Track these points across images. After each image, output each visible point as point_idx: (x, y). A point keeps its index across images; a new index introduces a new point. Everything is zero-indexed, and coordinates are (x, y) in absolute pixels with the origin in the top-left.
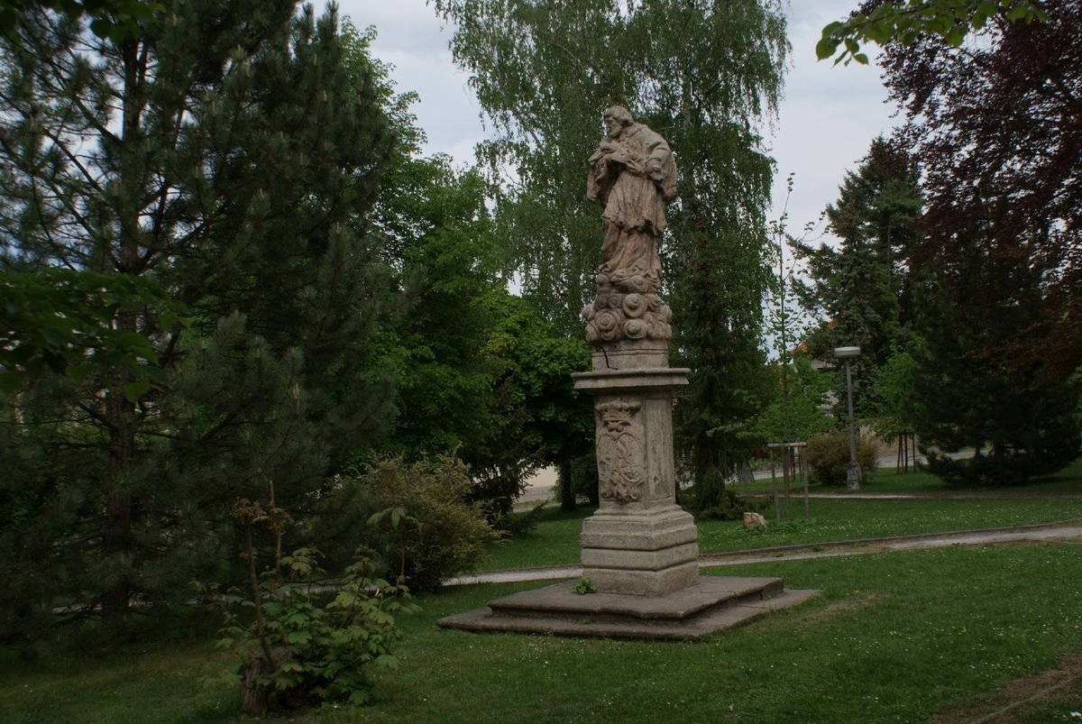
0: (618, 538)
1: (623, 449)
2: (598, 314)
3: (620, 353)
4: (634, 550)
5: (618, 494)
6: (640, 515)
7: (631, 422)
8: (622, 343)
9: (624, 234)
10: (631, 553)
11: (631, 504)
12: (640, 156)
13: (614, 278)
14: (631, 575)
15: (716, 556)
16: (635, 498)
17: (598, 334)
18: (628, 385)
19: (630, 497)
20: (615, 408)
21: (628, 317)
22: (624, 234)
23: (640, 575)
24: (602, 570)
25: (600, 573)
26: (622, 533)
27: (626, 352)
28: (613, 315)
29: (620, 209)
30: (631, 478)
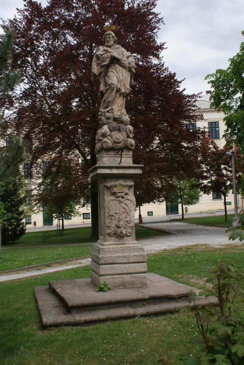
0: (124, 257)
1: (126, 207)
2: (113, 133)
4: (135, 263)
5: (121, 232)
7: (129, 193)
10: (132, 265)
11: (126, 238)
14: (132, 277)
15: (7, 272)
16: (129, 234)
17: (112, 144)
23: (138, 277)
24: (133, 275)
25: (113, 278)
26: (126, 254)
28: (122, 135)
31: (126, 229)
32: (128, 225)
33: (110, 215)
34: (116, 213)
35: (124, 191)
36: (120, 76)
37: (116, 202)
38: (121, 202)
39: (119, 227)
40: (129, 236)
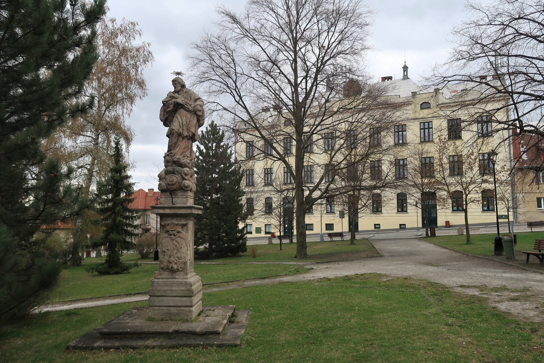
1: (177, 244)
2: (167, 176)
3: (177, 196)
4: (176, 297)
5: (172, 268)
6: (183, 278)
8: (178, 191)
9: (181, 139)
11: (178, 273)
12: (190, 103)
13: (175, 159)
16: (181, 270)
18: (183, 213)
19: (178, 269)
20: (174, 224)
21: (184, 179)
22: (181, 139)
23: (183, 310)
25: (160, 309)
27: (180, 196)
28: (176, 177)
29: (180, 126)
30: (179, 259)
31: (178, 265)
33: (163, 251)
34: (167, 250)
36: (184, 120)
37: (168, 239)
38: (173, 240)
39: (171, 263)
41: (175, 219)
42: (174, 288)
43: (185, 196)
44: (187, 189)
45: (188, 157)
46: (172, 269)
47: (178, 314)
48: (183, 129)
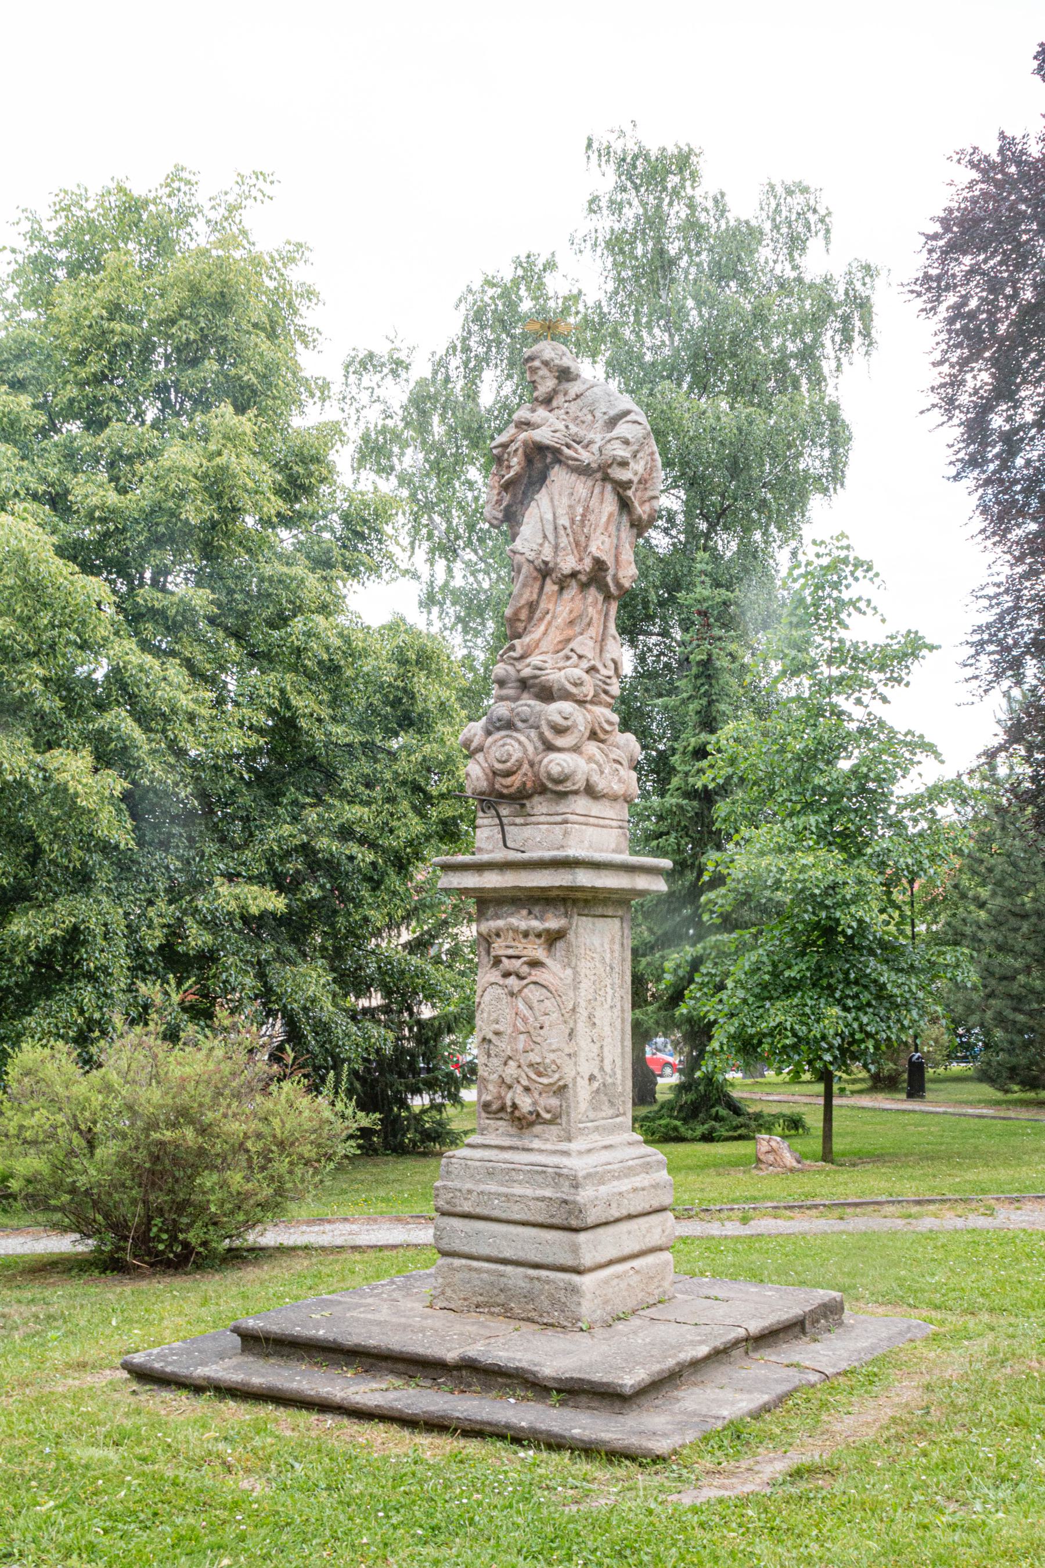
5: (515, 1106)
6: (555, 1152)
8: (537, 799)
9: (550, 587)
11: (538, 1129)
12: (591, 436)
16: (548, 1116)
20: (516, 930)
22: (550, 587)
23: (548, 1282)
25: (471, 1269)
27: (542, 819)
28: (520, 743)
29: (545, 537)
30: (540, 1074)
32: (541, 1080)
34: (497, 1033)
35: (525, 953)
37: (500, 991)
40: (546, 1122)
41: (524, 912)
42: (518, 1190)
43: (559, 819)
44: (560, 788)
45: (580, 657)
46: (517, 1114)
47: (529, 1297)
48: (556, 547)
